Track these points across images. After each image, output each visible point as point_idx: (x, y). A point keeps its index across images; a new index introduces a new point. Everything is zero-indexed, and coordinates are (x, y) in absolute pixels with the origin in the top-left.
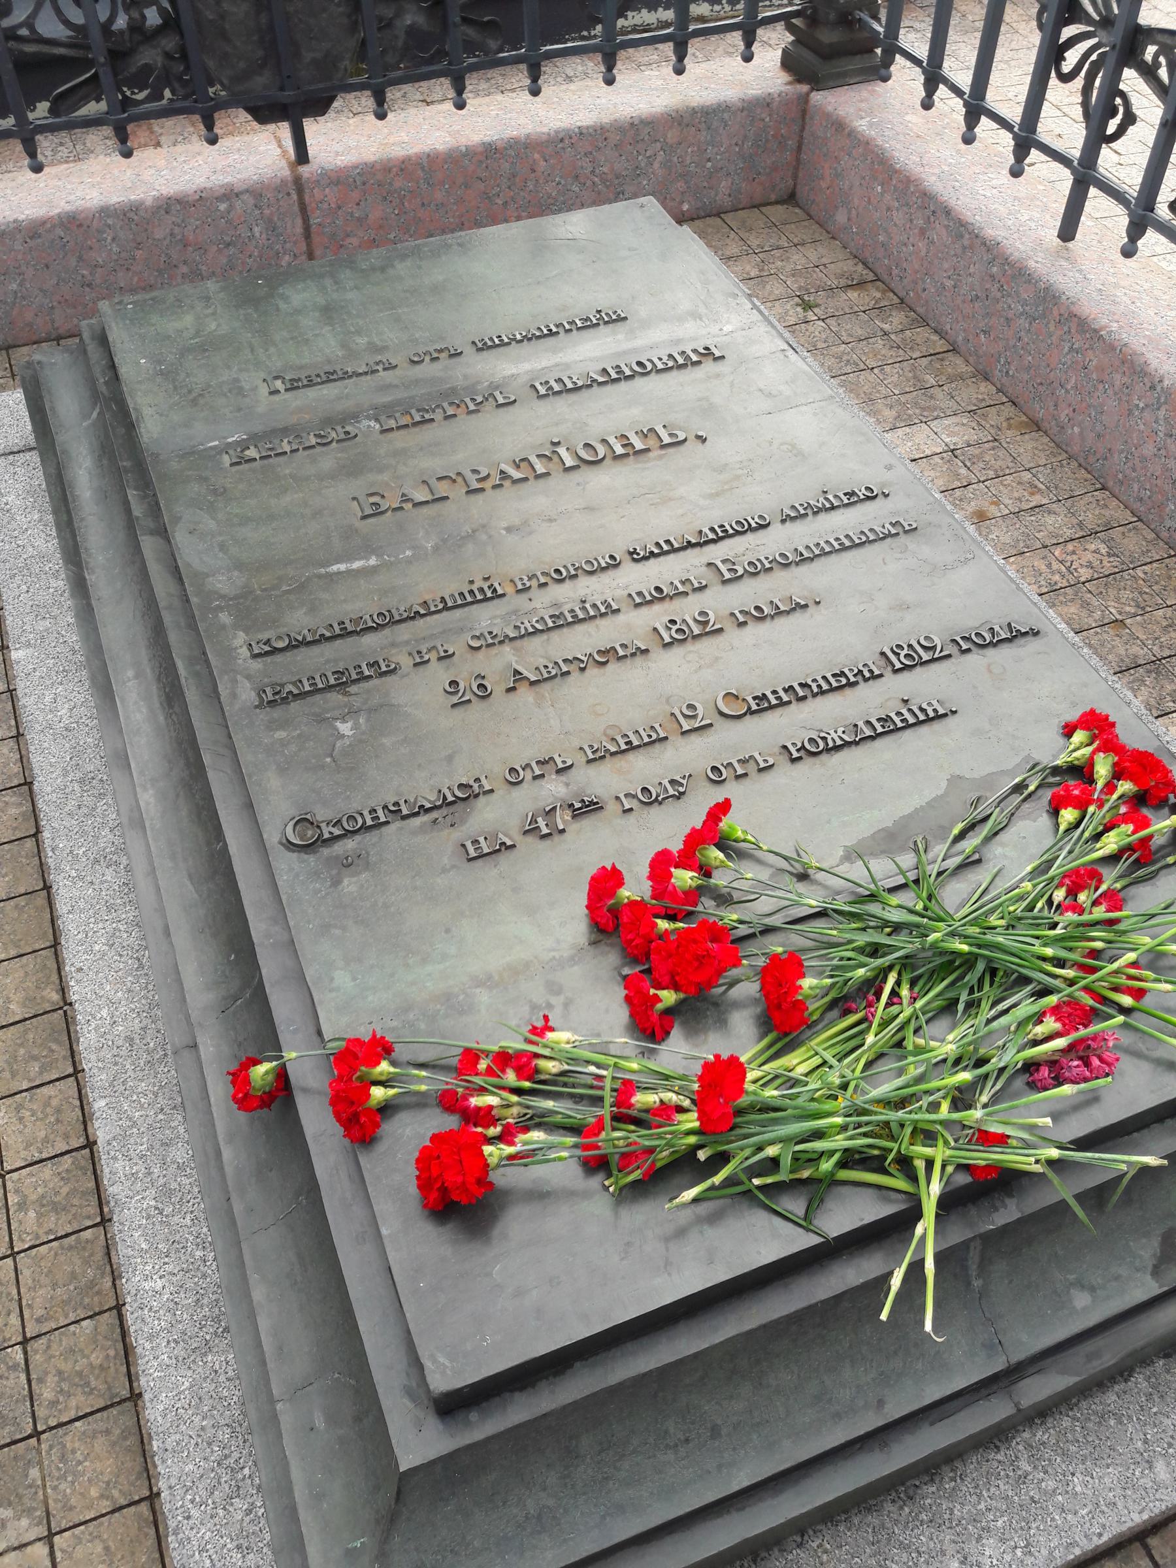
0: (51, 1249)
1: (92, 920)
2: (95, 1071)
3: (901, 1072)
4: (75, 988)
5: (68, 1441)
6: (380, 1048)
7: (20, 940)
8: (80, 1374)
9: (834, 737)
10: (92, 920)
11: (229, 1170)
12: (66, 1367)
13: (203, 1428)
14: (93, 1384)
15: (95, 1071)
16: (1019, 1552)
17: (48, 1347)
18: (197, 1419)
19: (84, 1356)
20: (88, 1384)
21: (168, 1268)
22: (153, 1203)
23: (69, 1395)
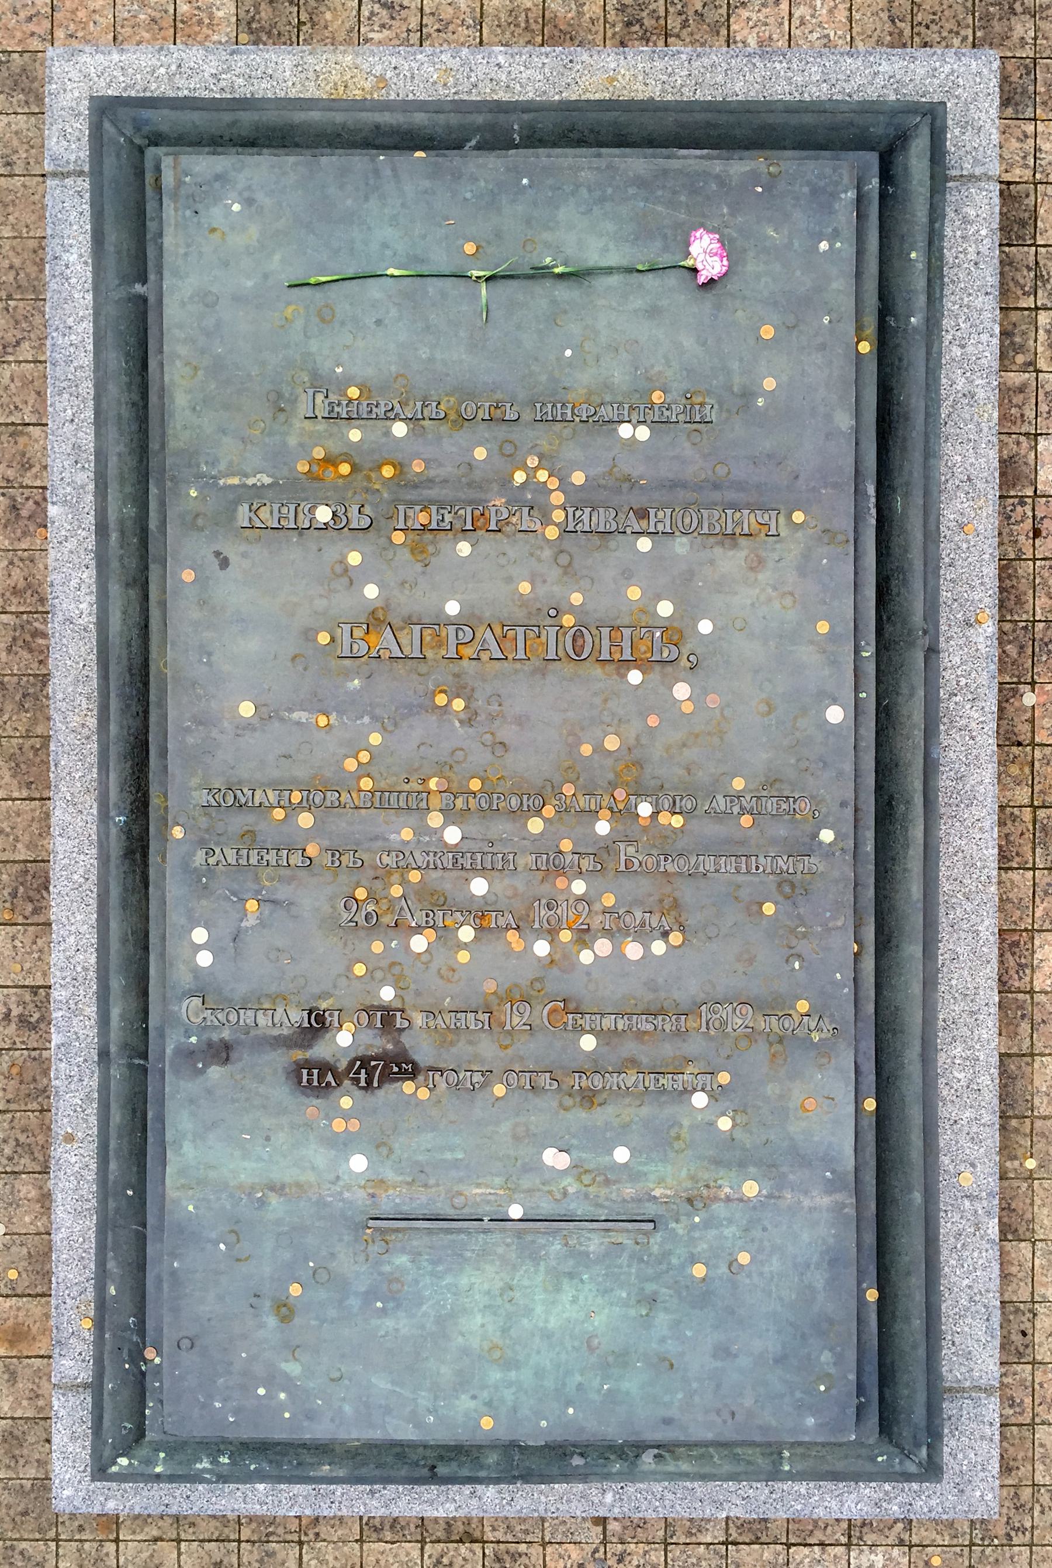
0: (22, 1055)
1: (76, 849)
2: (57, 985)
3: (430, 1557)
4: (54, 909)
5: (18, 1184)
6: (583, 213)
7: (32, 783)
8: (29, 1145)
9: (888, 628)
10: (76, 849)
11: (111, 1177)
12: (22, 1138)
13: (83, 1258)
14: (36, 1155)
15: (57, 985)
16: (505, 1502)
17: (12, 1121)
18: (80, 1251)
19: (33, 1135)
20: (32, 1153)
21: (82, 1151)
22: (80, 1102)
23: (20, 1157)
